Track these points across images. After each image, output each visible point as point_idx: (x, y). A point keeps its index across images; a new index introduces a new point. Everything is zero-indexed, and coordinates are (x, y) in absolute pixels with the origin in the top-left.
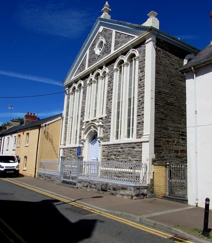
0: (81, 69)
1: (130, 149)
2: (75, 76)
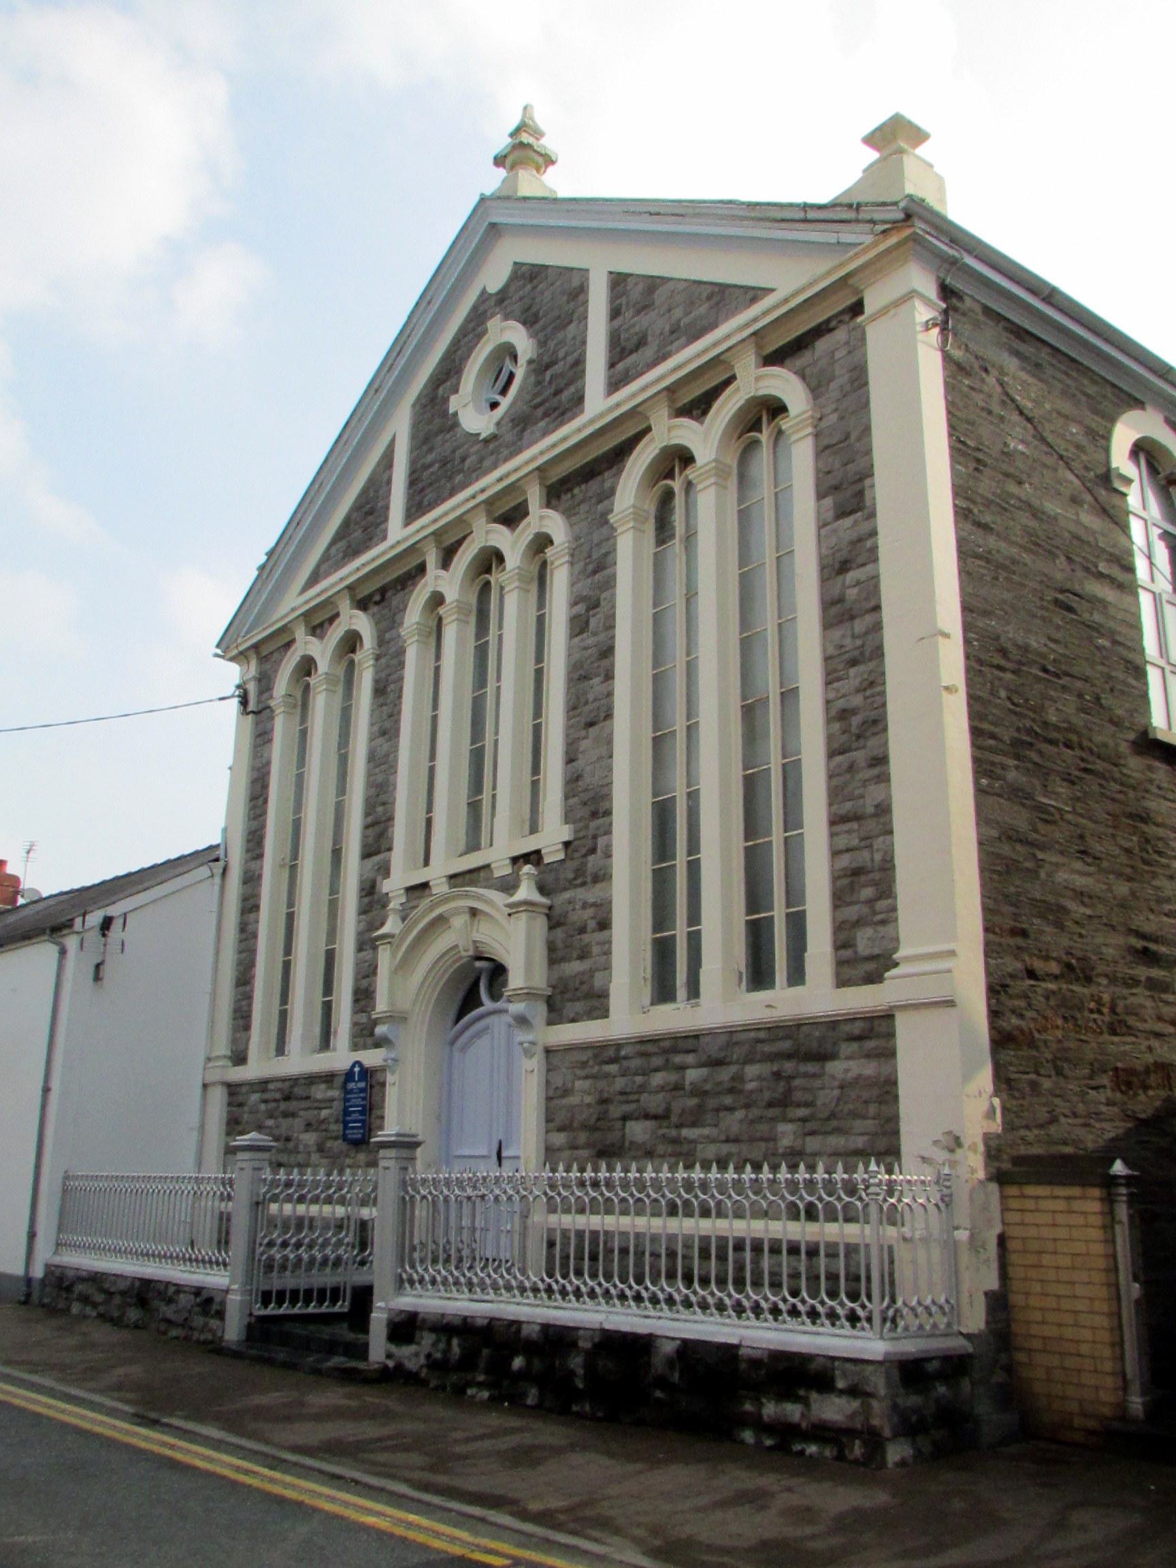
0: (357, 534)
1: (789, 1066)
2: (314, 579)
